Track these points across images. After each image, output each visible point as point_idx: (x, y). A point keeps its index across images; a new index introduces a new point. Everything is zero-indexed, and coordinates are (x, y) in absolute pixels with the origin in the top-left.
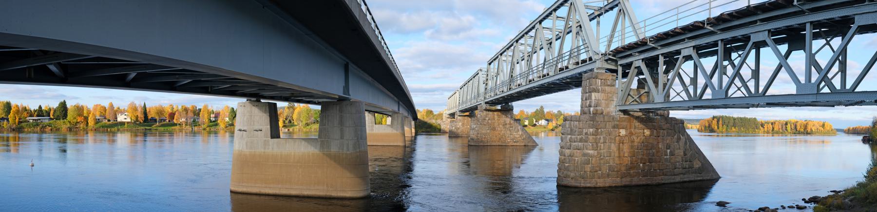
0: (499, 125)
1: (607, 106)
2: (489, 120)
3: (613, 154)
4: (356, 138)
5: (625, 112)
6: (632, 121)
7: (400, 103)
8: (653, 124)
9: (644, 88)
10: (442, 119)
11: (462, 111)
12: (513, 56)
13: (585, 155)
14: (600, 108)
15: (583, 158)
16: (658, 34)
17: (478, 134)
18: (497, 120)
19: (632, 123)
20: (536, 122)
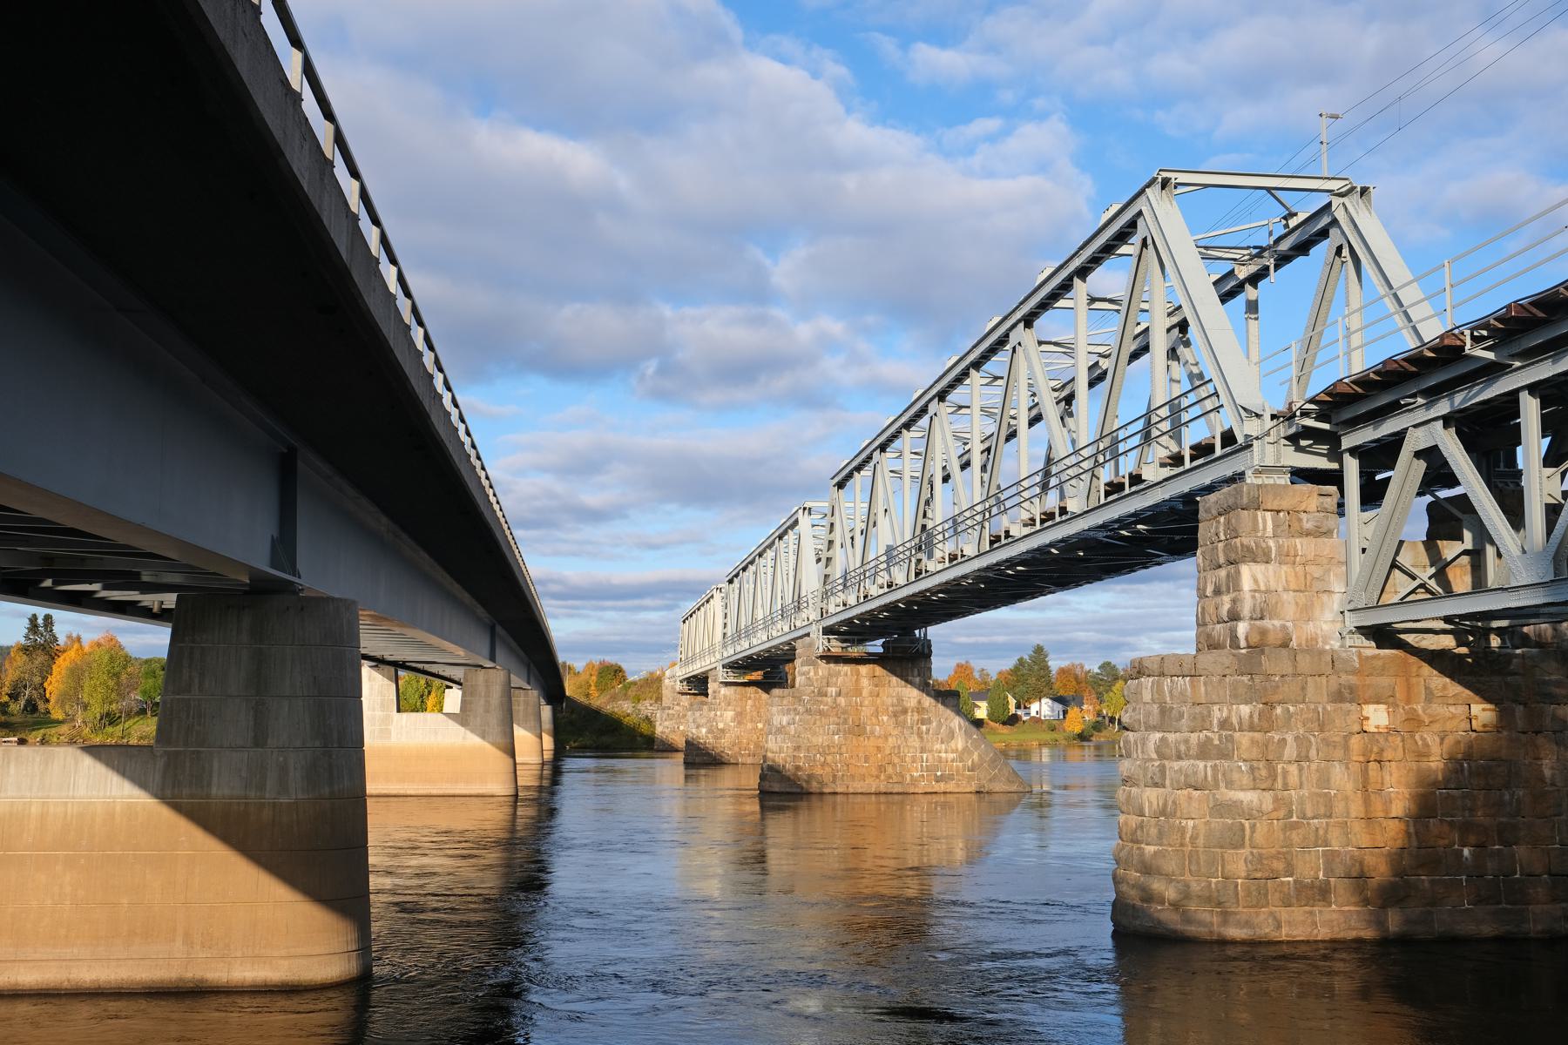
0: (876, 713)
1: (1306, 613)
2: (839, 694)
3: (1339, 807)
4: (317, 743)
5: (1383, 635)
6: (1414, 669)
7: (499, 629)
8: (1509, 679)
9: (1460, 538)
10: (659, 699)
11: (736, 666)
12: (925, 456)
13: (1221, 809)
14: (1277, 623)
15: (1217, 823)
16: (1508, 307)
17: (798, 748)
18: (871, 694)
19: (1414, 680)
20: (1018, 707)
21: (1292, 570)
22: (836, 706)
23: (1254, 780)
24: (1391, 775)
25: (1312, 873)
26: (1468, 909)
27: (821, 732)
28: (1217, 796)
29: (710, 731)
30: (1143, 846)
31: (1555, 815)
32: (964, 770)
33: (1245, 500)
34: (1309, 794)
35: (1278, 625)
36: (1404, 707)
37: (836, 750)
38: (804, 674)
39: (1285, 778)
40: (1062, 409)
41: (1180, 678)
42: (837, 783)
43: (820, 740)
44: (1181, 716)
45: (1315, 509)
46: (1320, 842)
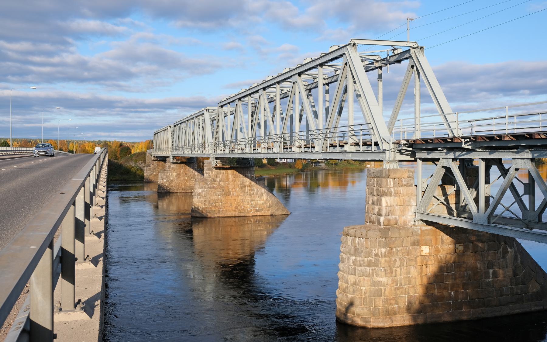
0: (235, 188)
1: (403, 212)
2: (221, 181)
3: (413, 281)
6: (438, 233)
10: (145, 161)
13: (374, 284)
14: (393, 217)
17: (206, 201)
18: (232, 180)
19: (438, 237)
21: (399, 198)
22: (219, 185)
23: (386, 274)
24: (430, 269)
25: (404, 304)
26: (452, 312)
27: (214, 195)
28: (373, 280)
29: (167, 181)
30: (347, 294)
31: (481, 279)
32: (266, 207)
33: (384, 175)
34: (403, 277)
35: (394, 218)
36: (434, 246)
37: (220, 201)
38: (208, 173)
39: (396, 272)
40: (307, 93)
41: (362, 239)
42: (220, 213)
43: (214, 198)
44: (362, 252)
45: (407, 177)
46: (406, 293)
